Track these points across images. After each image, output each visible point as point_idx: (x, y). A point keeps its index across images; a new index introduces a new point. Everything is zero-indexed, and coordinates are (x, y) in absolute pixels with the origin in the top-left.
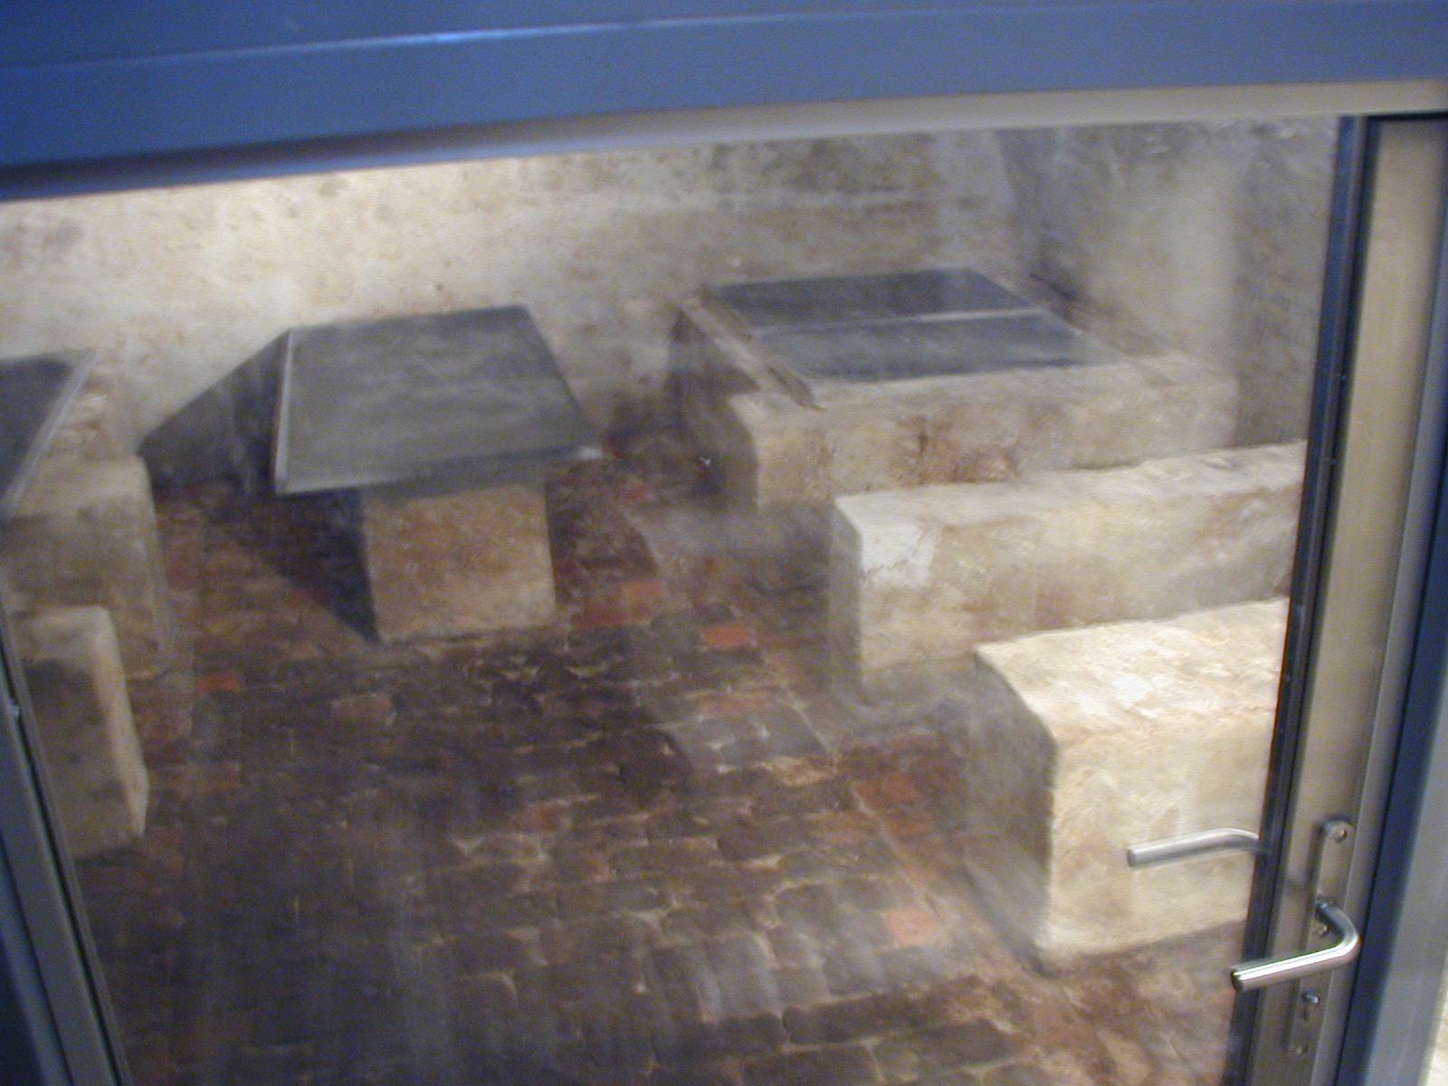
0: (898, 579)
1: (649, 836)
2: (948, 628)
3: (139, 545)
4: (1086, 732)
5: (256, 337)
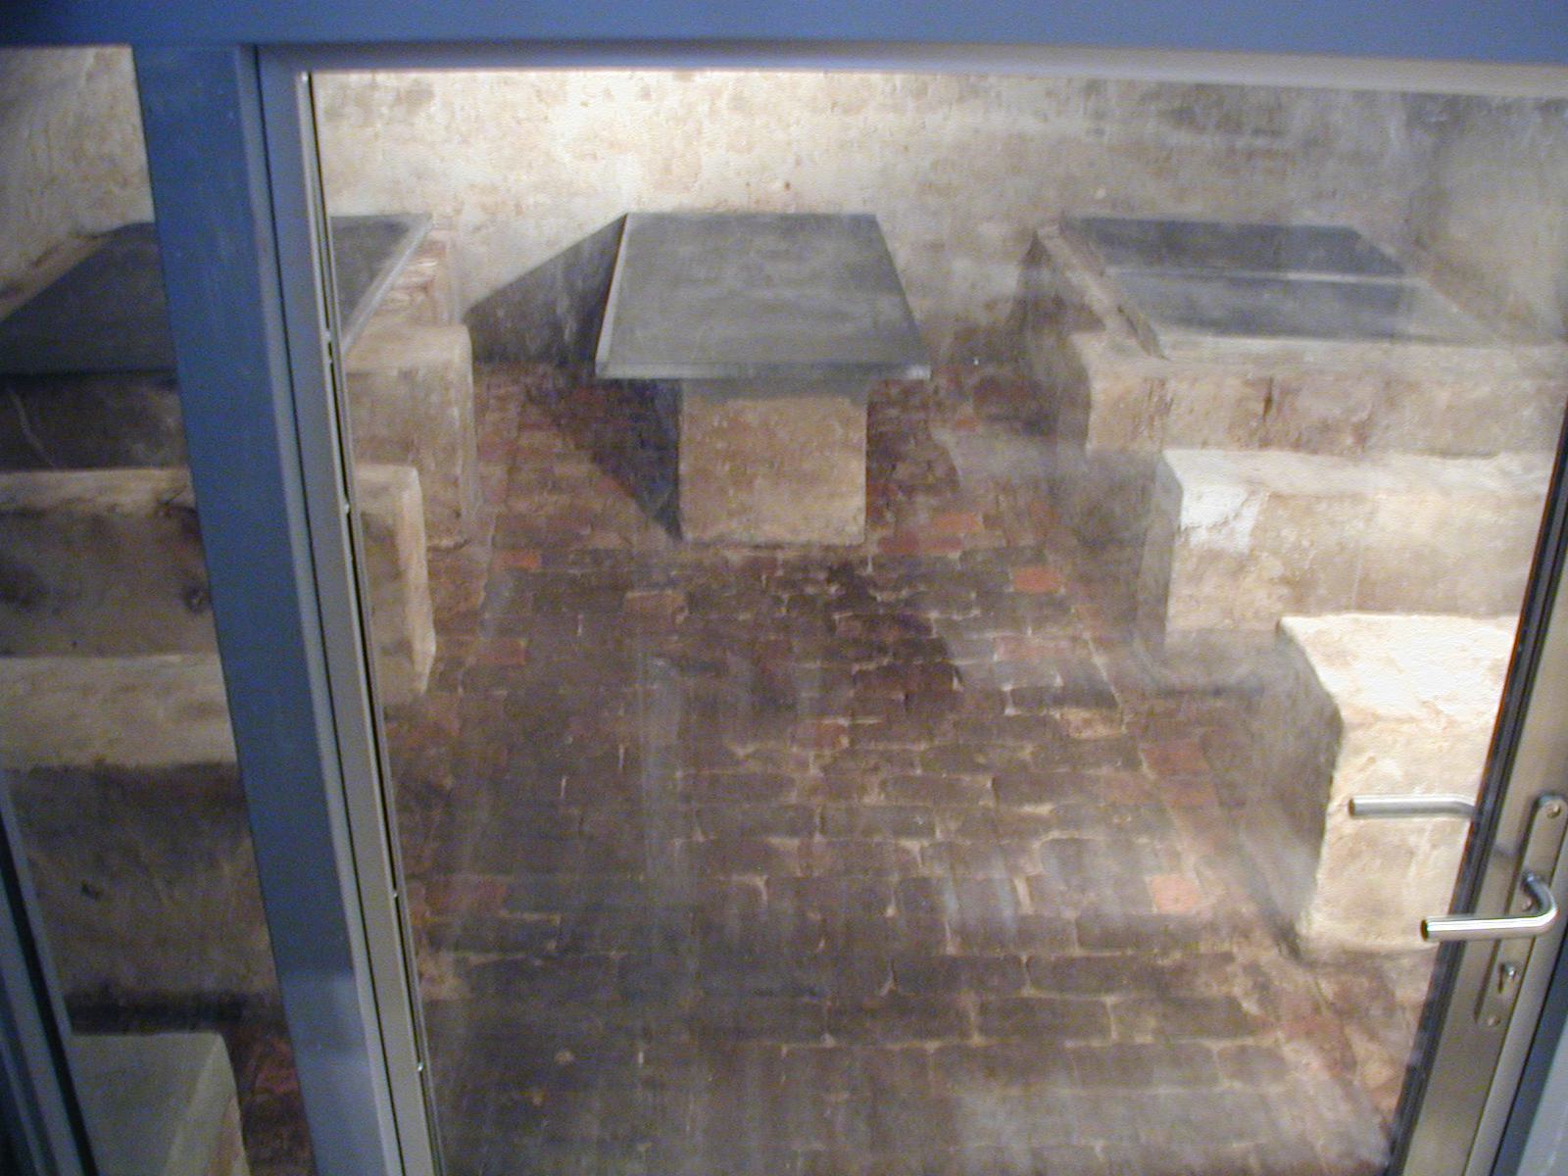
0: (1220, 541)
1: (925, 766)
2: (1258, 596)
3: (455, 412)
4: (1378, 718)
5: (600, 219)
